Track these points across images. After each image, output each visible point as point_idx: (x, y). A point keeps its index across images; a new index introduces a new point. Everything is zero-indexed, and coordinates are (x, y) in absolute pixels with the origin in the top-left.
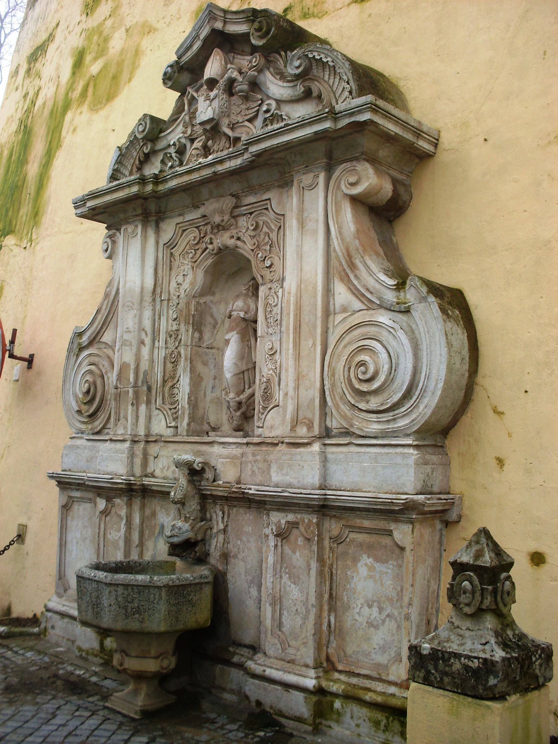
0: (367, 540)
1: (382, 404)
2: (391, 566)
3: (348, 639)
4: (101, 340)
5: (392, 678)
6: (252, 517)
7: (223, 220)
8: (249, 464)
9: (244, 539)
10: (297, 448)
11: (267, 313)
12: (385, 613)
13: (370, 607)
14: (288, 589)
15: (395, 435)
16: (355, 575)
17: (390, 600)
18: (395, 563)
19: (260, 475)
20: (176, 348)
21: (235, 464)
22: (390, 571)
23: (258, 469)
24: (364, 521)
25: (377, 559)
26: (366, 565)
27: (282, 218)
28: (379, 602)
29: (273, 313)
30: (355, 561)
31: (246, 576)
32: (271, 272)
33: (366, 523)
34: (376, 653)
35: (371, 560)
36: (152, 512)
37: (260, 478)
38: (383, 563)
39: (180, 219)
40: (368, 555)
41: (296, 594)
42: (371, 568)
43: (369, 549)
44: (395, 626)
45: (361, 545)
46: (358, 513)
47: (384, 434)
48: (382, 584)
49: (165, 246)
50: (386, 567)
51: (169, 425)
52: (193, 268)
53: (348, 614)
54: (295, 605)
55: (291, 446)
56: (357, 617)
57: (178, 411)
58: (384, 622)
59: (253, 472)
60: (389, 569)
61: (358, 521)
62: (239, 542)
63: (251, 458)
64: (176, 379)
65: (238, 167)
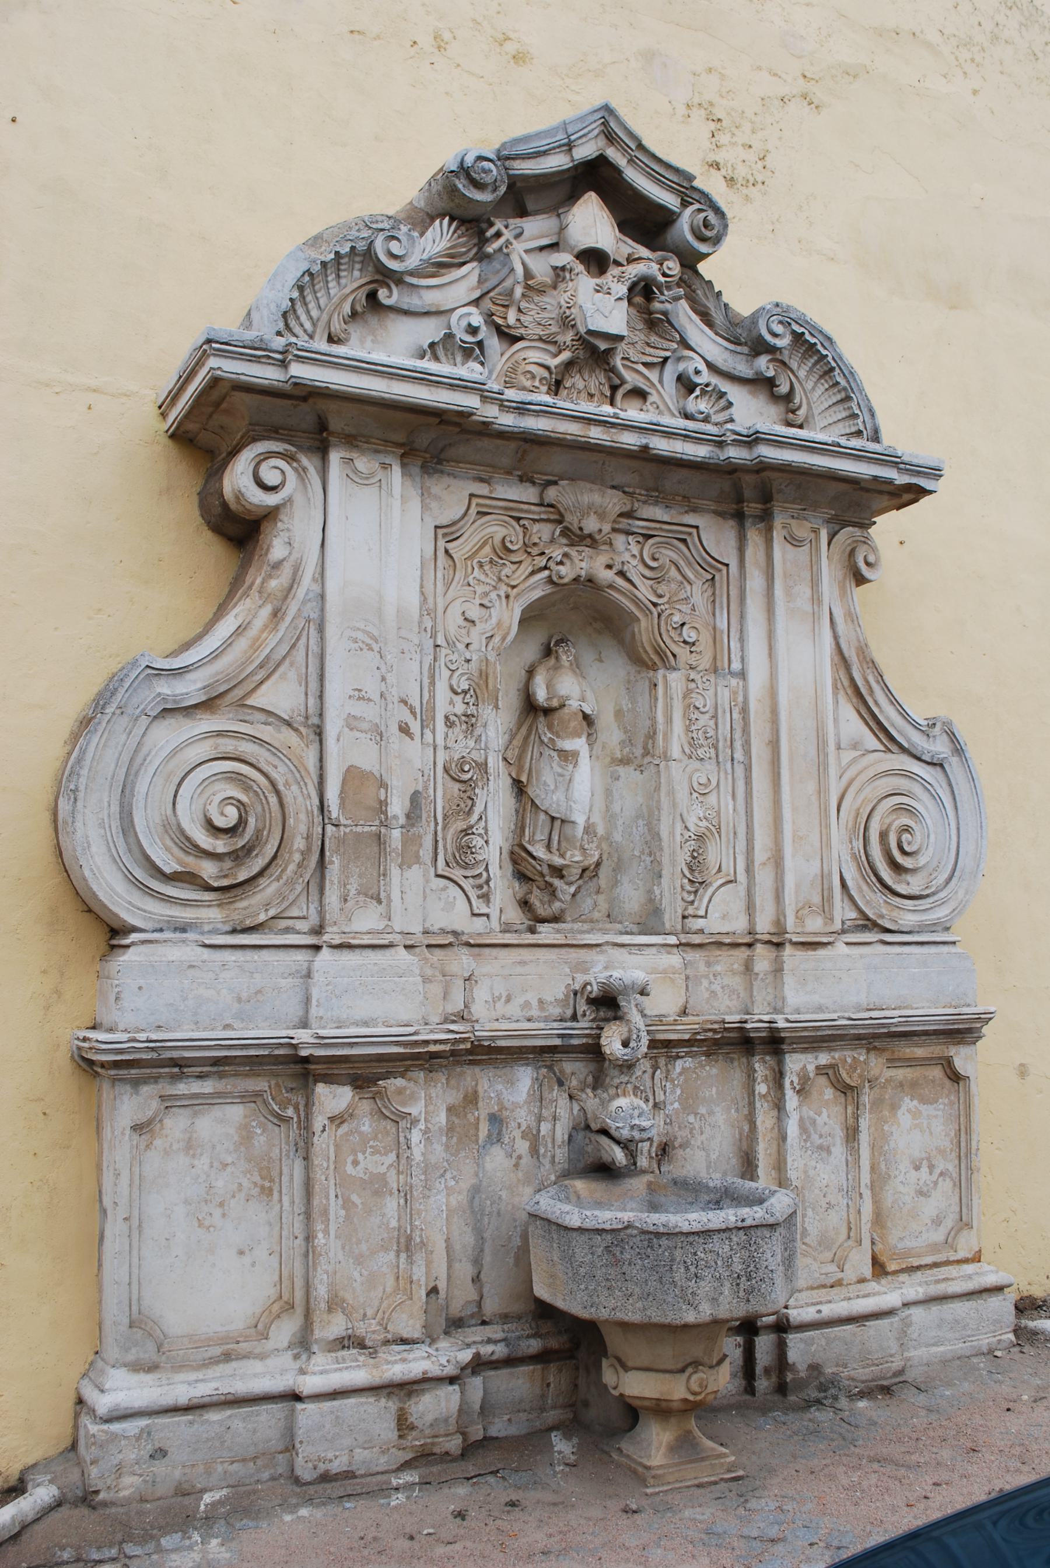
0: (910, 1076)
2: (941, 1107)
3: (889, 1224)
6: (714, 1071)
8: (703, 980)
9: (702, 1110)
10: (815, 950)
12: (937, 1171)
13: (917, 1168)
14: (811, 1173)
16: (894, 1129)
17: (941, 1152)
19: (726, 997)
21: (672, 980)
22: (940, 1113)
23: (722, 988)
24: (916, 1049)
25: (923, 1101)
28: (928, 1159)
30: (894, 1107)
31: (709, 1174)
32: (691, 652)
33: (920, 1052)
34: (928, 1231)
35: (915, 1102)
36: (465, 1097)
37: (728, 1003)
38: (931, 1104)
39: (482, 489)
40: (912, 1096)
41: (826, 1177)
42: (915, 1114)
46: (916, 1038)
48: (931, 1133)
50: (935, 1109)
51: (476, 911)
52: (507, 597)
53: (887, 1188)
55: (800, 947)
56: (901, 1188)
58: (936, 1183)
59: (713, 993)
61: (908, 1050)
62: (691, 1119)
63: (702, 968)
65: (699, 459)
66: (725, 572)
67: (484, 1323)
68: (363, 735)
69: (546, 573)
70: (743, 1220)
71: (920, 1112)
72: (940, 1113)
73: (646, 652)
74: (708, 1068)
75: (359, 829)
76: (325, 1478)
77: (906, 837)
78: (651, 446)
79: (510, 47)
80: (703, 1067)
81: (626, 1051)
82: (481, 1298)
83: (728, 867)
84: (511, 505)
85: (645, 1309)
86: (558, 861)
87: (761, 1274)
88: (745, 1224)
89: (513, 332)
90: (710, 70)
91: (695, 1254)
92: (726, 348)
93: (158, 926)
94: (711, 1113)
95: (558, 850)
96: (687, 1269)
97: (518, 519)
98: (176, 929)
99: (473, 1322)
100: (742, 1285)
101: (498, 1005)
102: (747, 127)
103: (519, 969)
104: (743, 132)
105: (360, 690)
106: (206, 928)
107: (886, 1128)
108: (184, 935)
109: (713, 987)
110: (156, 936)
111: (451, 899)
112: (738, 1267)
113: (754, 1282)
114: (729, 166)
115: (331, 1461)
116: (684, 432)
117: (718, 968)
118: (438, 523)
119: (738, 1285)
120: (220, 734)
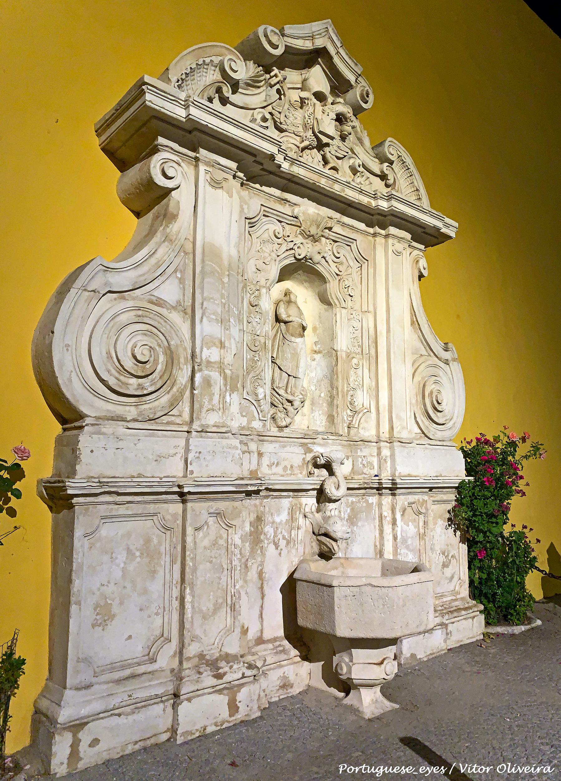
66: (366, 263)
69: (293, 252)
73: (332, 298)
83: (366, 405)
84: (133, 519)
89: (282, 126)
95: (291, 392)
97: (280, 222)
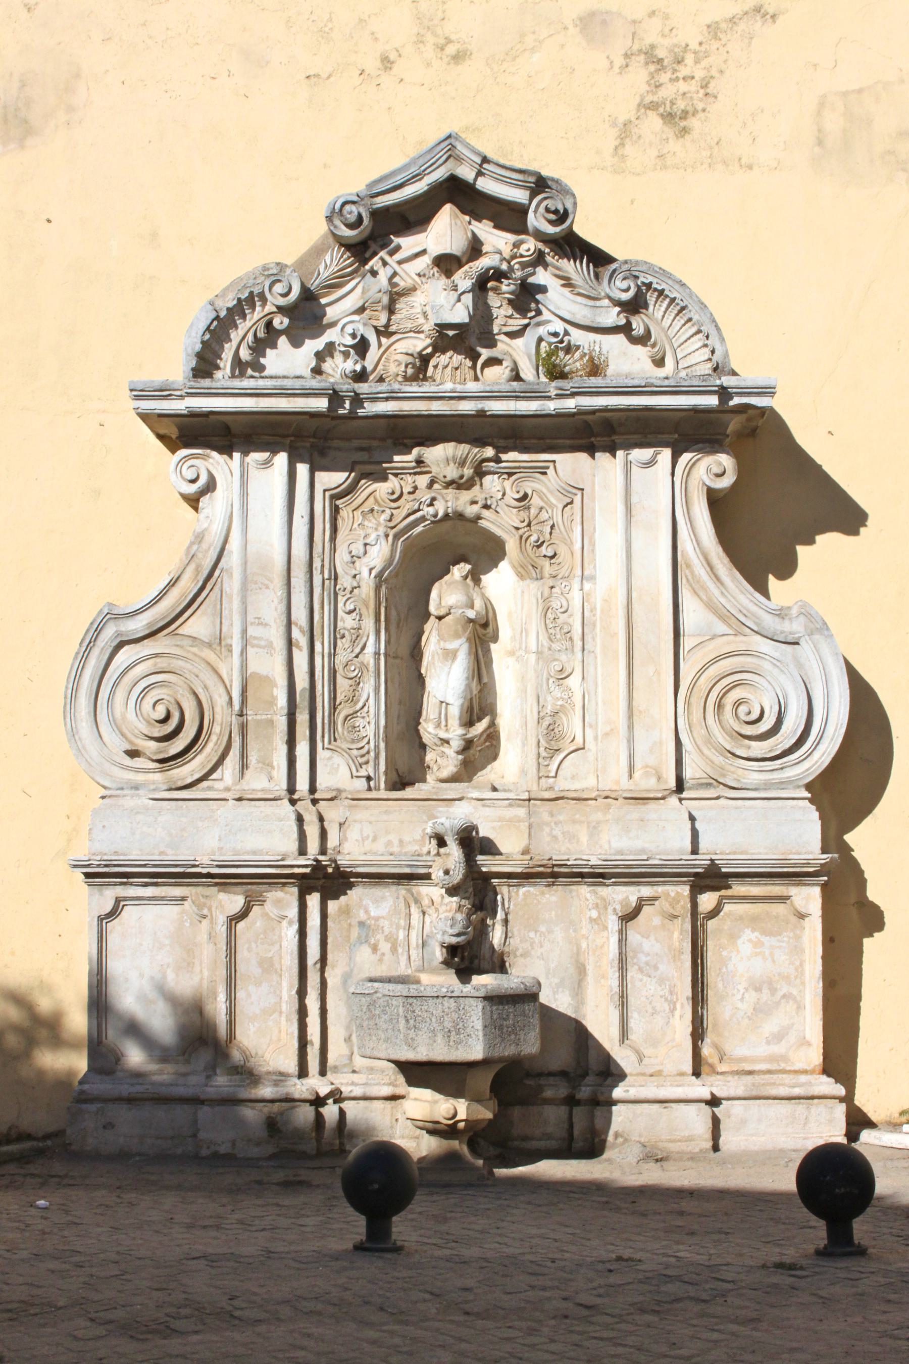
1: (770, 751)
2: (785, 939)
4: (180, 631)
5: (798, 1066)
7: (462, 477)
9: (543, 929)
11: (548, 621)
12: (780, 994)
13: (758, 989)
15: (782, 786)
18: (791, 934)
20: (357, 656)
23: (563, 833)
25: (765, 933)
26: (750, 941)
27: (579, 493)
29: (559, 621)
35: (757, 934)
41: (653, 988)
42: (758, 944)
43: (754, 921)
44: (795, 1007)
45: (741, 918)
47: (768, 786)
48: (774, 961)
49: (327, 494)
50: (779, 941)
54: (650, 1003)
56: (739, 1005)
57: (368, 752)
59: (555, 838)
60: (783, 942)
62: (532, 935)
64: (360, 704)
67: (354, 1072)
68: (261, 650)
70: (452, 992)
71: (763, 944)
72: (784, 944)
74: (547, 896)
75: (259, 717)
76: (216, 1156)
77: (743, 709)
78: (486, 409)
79: (451, 49)
80: (543, 893)
81: (447, 877)
82: (352, 1054)
85: (386, 1049)
86: (443, 735)
87: (468, 1030)
88: (453, 995)
90: (653, 13)
91: (414, 1012)
92: (586, 305)
93: (120, 786)
94: (550, 932)
96: (407, 1021)
98: (132, 788)
99: (346, 1070)
100: (452, 1038)
101: (366, 843)
102: (689, 59)
103: (385, 817)
104: (686, 65)
105: (259, 618)
106: (152, 787)
107: (725, 953)
108: (137, 792)
109: (554, 833)
110: (119, 792)
111: (336, 766)
112: (448, 1024)
113: (462, 1036)
114: (668, 102)
115: (219, 1145)
116: (514, 394)
117: (561, 818)
118: (325, 488)
119: (449, 1037)
120: (157, 655)
